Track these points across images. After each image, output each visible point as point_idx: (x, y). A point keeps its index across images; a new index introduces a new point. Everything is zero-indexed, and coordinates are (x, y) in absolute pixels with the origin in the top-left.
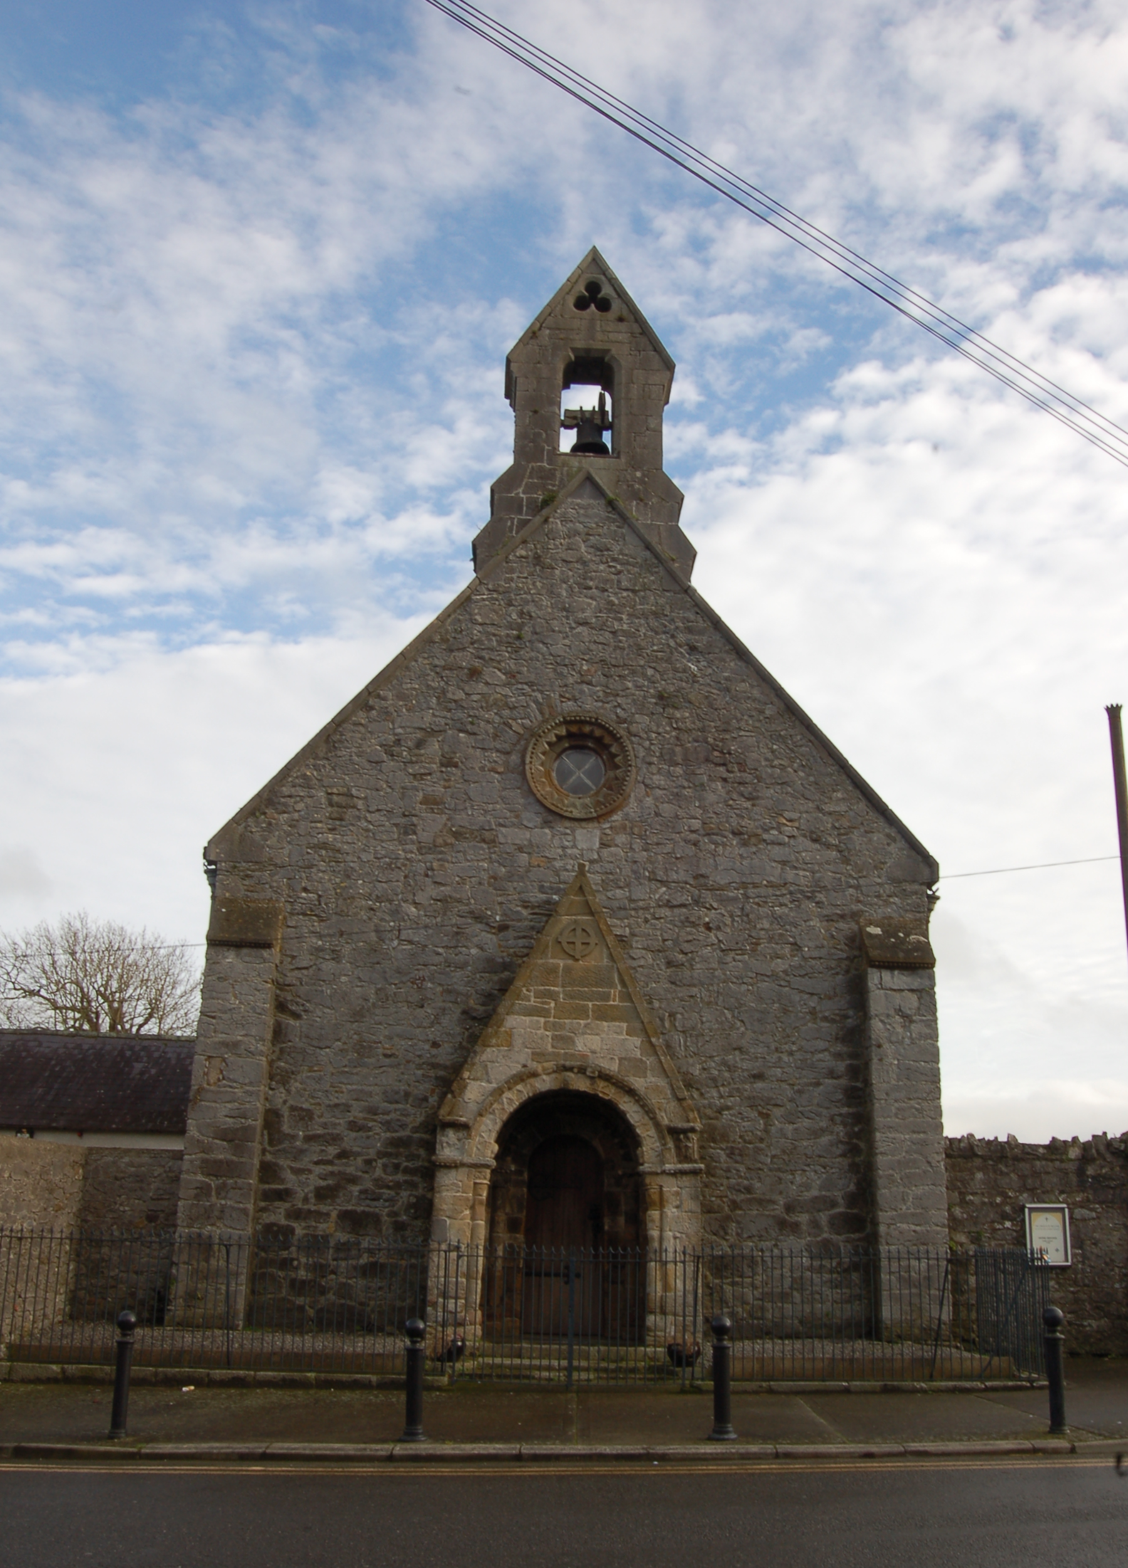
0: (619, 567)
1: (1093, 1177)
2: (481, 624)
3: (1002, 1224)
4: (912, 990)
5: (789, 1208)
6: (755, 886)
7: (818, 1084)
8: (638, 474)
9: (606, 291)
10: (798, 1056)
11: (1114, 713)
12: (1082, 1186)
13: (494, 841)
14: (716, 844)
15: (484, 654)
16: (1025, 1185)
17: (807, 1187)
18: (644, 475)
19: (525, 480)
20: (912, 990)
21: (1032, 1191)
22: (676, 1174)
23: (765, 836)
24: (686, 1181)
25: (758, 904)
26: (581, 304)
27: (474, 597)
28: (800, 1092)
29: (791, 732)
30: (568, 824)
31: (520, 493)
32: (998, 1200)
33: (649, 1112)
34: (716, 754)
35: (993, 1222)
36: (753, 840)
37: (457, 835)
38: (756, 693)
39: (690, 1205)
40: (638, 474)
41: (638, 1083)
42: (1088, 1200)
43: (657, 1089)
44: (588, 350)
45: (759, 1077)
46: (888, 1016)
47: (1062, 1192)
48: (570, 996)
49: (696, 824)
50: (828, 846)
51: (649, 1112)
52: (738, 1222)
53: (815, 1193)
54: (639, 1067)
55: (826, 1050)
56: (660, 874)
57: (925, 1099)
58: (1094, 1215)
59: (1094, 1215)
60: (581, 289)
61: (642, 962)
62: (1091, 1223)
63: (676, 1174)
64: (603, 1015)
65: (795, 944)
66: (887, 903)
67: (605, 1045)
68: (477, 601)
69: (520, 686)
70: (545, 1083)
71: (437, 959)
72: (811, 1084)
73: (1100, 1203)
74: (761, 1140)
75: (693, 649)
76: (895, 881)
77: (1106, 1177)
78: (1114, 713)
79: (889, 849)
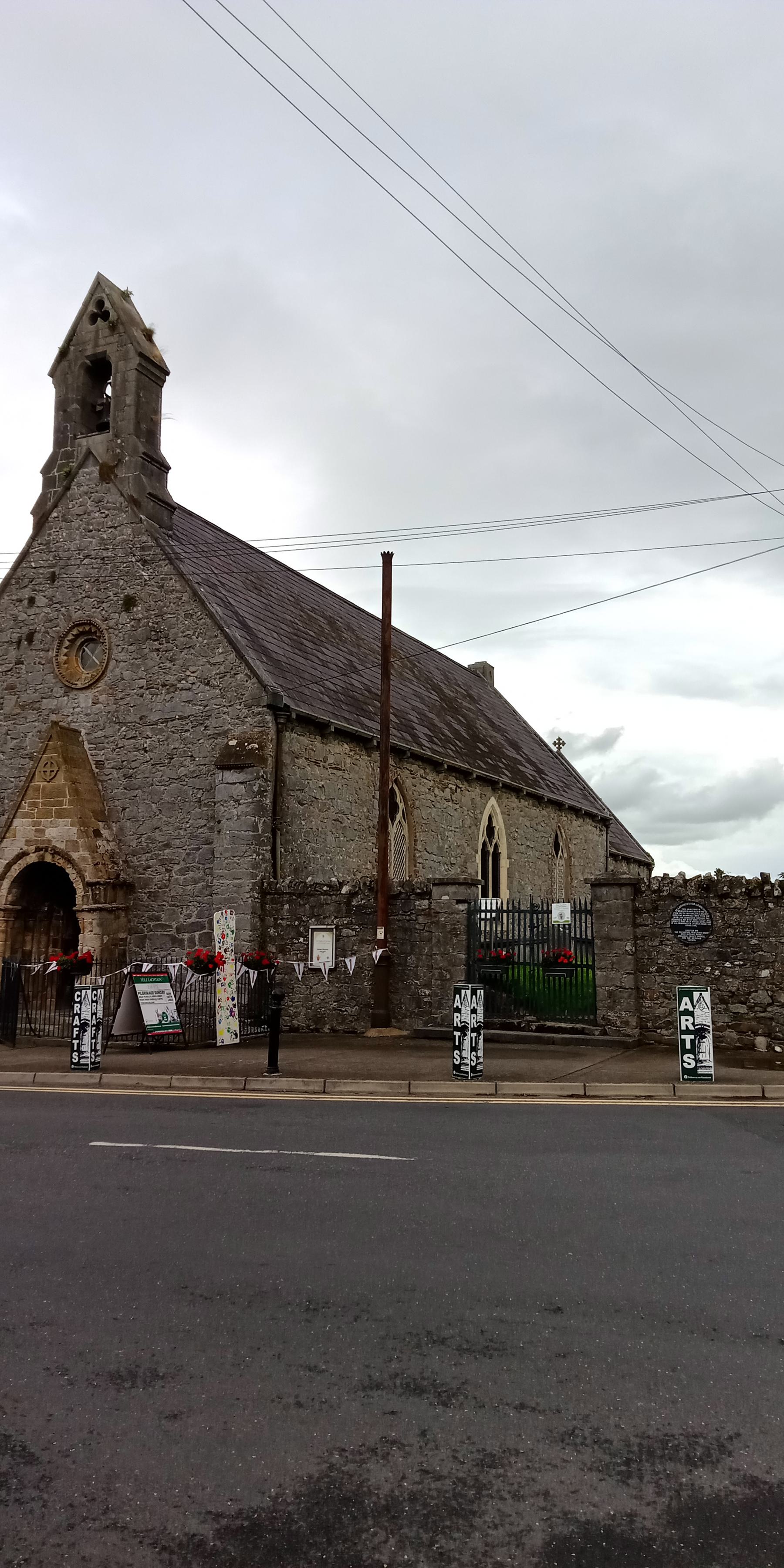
0: (107, 512)
1: (356, 907)
2: (35, 568)
3: (298, 939)
4: (240, 783)
5: (178, 930)
6: (172, 720)
7: (199, 849)
8: (119, 441)
9: (92, 308)
10: (189, 830)
11: (387, 558)
12: (348, 913)
13: (39, 708)
14: (153, 695)
15: (37, 588)
16: (313, 913)
17: (189, 916)
18: (122, 441)
19: (59, 462)
20: (240, 783)
21: (317, 917)
22: (89, 911)
23: (179, 685)
24: (95, 915)
25: (173, 732)
26: (93, 318)
27: (31, 551)
28: (188, 854)
29: (196, 610)
30: (75, 692)
31: (55, 473)
32: (297, 923)
33: (80, 873)
34: (153, 633)
35: (292, 938)
36: (172, 690)
37: (23, 707)
38: (178, 586)
39: (97, 930)
40: (119, 441)
41: (75, 856)
42: (352, 923)
43: (84, 859)
44: (95, 355)
45: (168, 846)
46: (226, 801)
47: (336, 918)
48: (44, 804)
49: (143, 682)
50: (214, 687)
51: (80, 873)
52: (150, 940)
53: (193, 920)
54: (75, 845)
55: (205, 825)
56: (121, 719)
57: (242, 856)
58: (354, 933)
59: (354, 933)
60: (92, 308)
61: (110, 777)
62: (353, 938)
63: (89, 911)
64: (60, 815)
65: (192, 756)
66: (244, 723)
67: (60, 832)
68: (33, 553)
69: (55, 605)
70: (32, 858)
71: (13, 785)
72: (193, 849)
73: (359, 925)
74: (166, 887)
75: (145, 562)
76: (248, 707)
77: (364, 906)
78: (387, 558)
79: (247, 684)
